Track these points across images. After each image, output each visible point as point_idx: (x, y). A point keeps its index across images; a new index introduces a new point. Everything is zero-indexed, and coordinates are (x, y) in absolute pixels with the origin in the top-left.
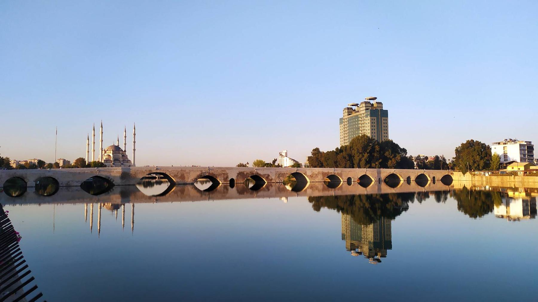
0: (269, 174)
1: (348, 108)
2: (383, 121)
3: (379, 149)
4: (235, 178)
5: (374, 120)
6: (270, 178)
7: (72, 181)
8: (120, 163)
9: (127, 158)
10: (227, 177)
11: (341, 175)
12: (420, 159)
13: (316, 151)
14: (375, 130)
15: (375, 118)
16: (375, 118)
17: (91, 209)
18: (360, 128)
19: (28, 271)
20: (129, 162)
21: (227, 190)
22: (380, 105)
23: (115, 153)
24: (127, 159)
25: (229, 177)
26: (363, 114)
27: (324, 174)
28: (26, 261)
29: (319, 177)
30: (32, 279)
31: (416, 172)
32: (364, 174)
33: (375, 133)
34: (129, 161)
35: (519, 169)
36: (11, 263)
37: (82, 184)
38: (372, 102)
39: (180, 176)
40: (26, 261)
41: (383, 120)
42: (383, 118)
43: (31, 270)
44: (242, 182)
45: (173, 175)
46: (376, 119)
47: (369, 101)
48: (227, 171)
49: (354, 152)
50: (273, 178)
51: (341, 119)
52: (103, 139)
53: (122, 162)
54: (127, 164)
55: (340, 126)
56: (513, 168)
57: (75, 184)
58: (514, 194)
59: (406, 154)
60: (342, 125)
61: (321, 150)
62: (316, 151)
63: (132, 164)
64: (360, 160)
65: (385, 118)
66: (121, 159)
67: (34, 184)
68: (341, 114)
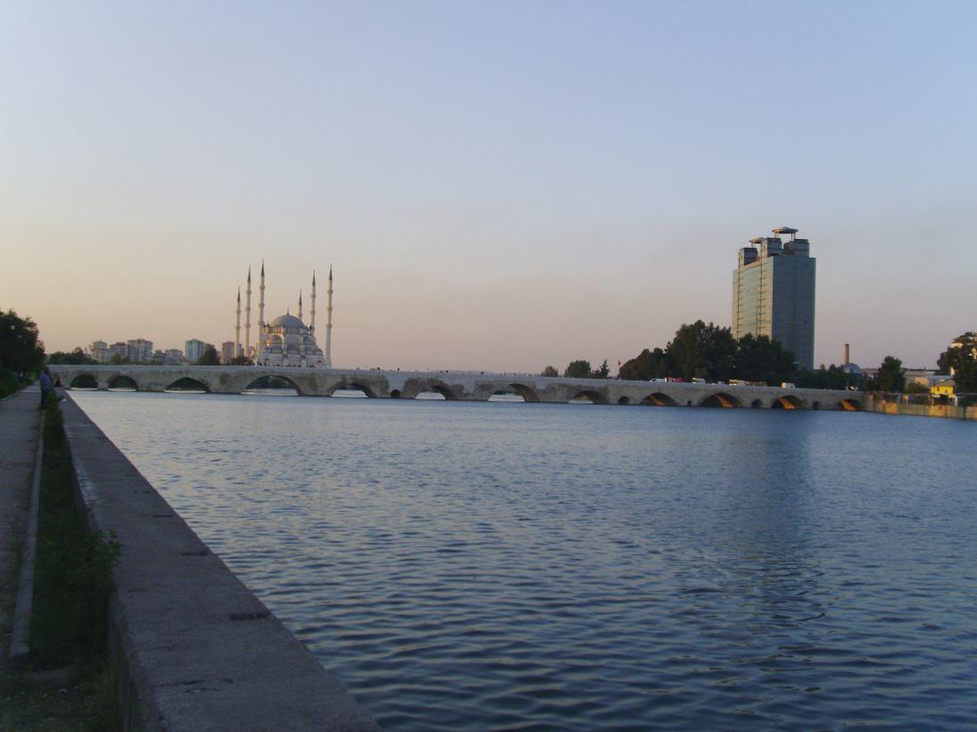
3: (872, 377)
7: (155, 383)
8: (298, 356)
9: (314, 344)
10: (387, 387)
12: (104, 350)
20: (318, 353)
23: (291, 333)
24: (313, 347)
34: (317, 351)
36: (752, 377)
48: (388, 378)
52: (333, 288)
53: (303, 354)
54: (314, 357)
58: (965, 412)
63: (325, 357)
66: (302, 347)
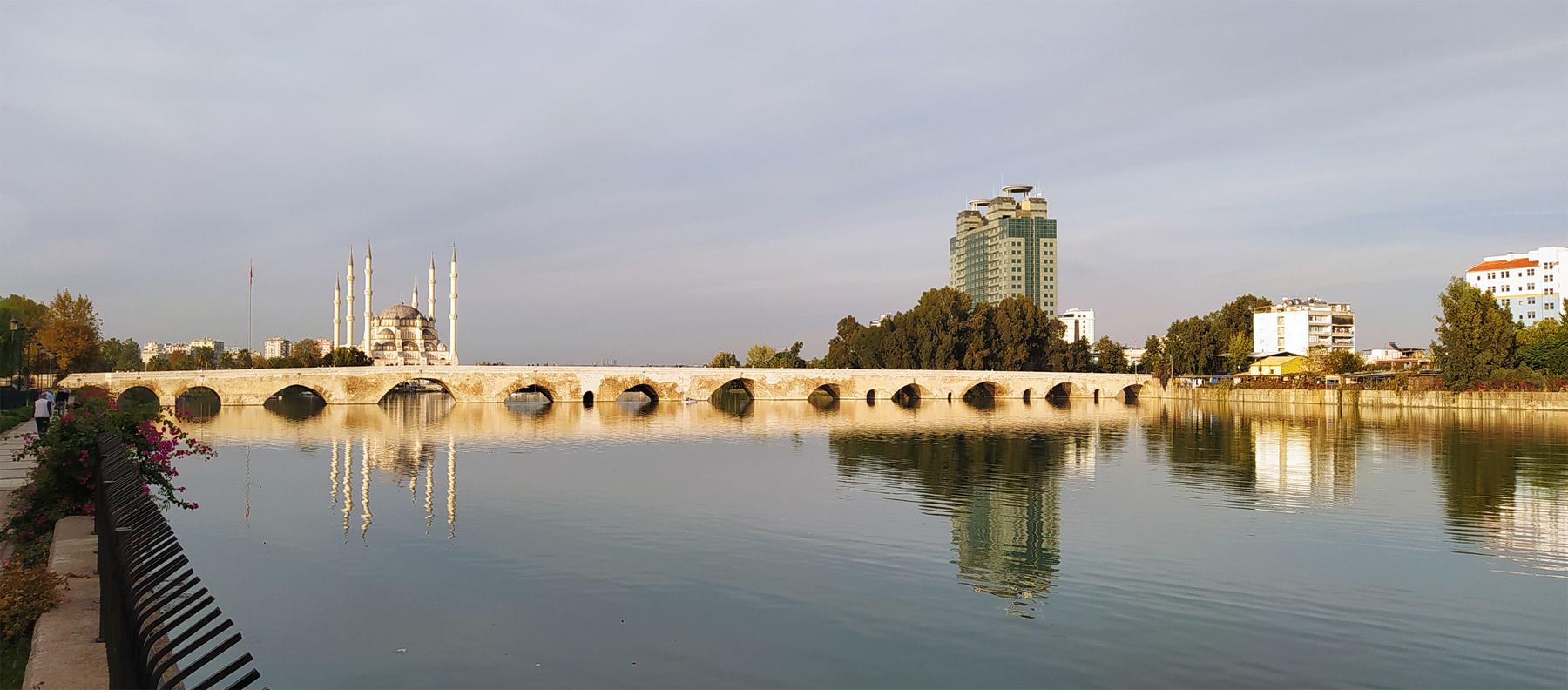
0: (677, 382)
1: (968, 213)
2: (1042, 248)
4: (595, 391)
5: (1019, 244)
6: (678, 390)
10: (578, 389)
11: (850, 384)
13: (848, 325)
14: (1019, 270)
15: (1022, 240)
16: (1022, 240)
17: (345, 469)
18: (989, 265)
19: (200, 589)
21: (577, 413)
22: (1040, 206)
25: (582, 387)
26: (996, 228)
27: (807, 383)
28: (200, 580)
29: (797, 388)
30: (237, 638)
31: (1050, 380)
32: (911, 382)
33: (1019, 278)
35: (1272, 371)
37: (266, 402)
38: (1018, 197)
39: (471, 385)
40: (200, 580)
41: (1042, 244)
42: (1043, 241)
43: (214, 596)
44: (612, 399)
45: (457, 385)
46: (1023, 244)
47: (1010, 195)
49: (922, 330)
50: (686, 390)
51: (953, 241)
55: (950, 257)
56: (1260, 370)
57: (253, 401)
59: (1063, 335)
60: (955, 256)
61: (864, 321)
62: (848, 325)
64: (934, 350)
65: (1048, 240)
67: (172, 401)
68: (951, 228)
